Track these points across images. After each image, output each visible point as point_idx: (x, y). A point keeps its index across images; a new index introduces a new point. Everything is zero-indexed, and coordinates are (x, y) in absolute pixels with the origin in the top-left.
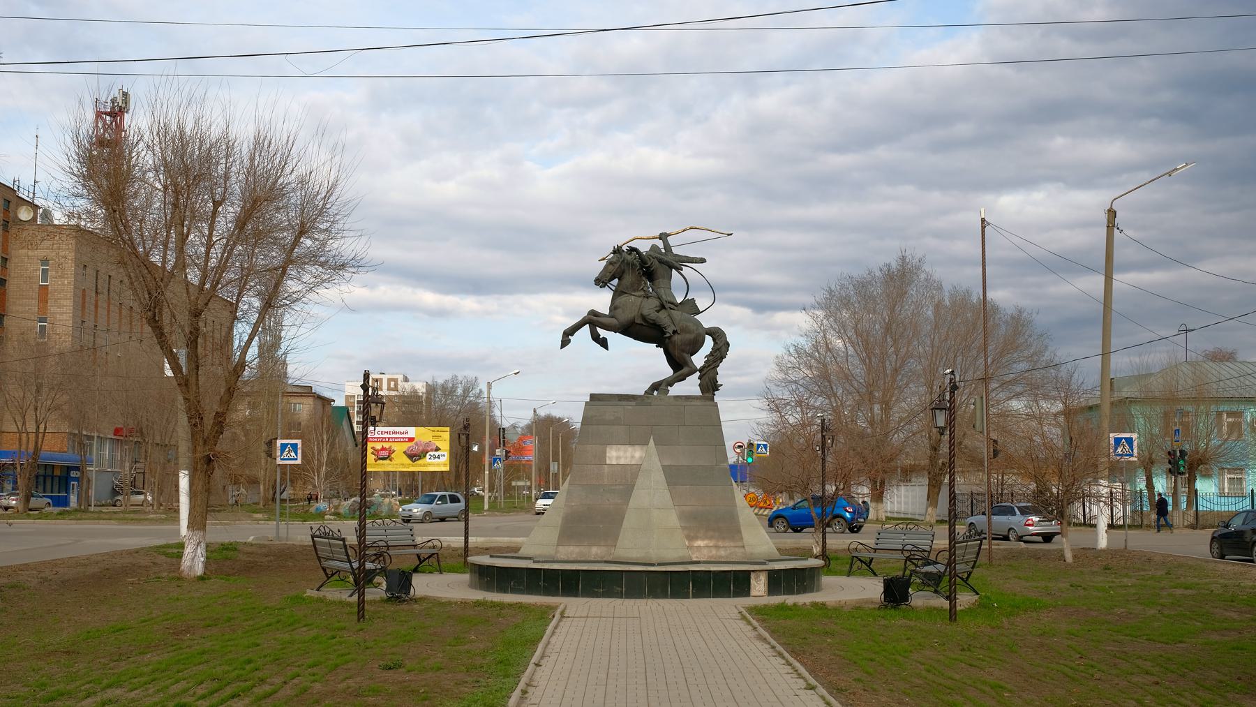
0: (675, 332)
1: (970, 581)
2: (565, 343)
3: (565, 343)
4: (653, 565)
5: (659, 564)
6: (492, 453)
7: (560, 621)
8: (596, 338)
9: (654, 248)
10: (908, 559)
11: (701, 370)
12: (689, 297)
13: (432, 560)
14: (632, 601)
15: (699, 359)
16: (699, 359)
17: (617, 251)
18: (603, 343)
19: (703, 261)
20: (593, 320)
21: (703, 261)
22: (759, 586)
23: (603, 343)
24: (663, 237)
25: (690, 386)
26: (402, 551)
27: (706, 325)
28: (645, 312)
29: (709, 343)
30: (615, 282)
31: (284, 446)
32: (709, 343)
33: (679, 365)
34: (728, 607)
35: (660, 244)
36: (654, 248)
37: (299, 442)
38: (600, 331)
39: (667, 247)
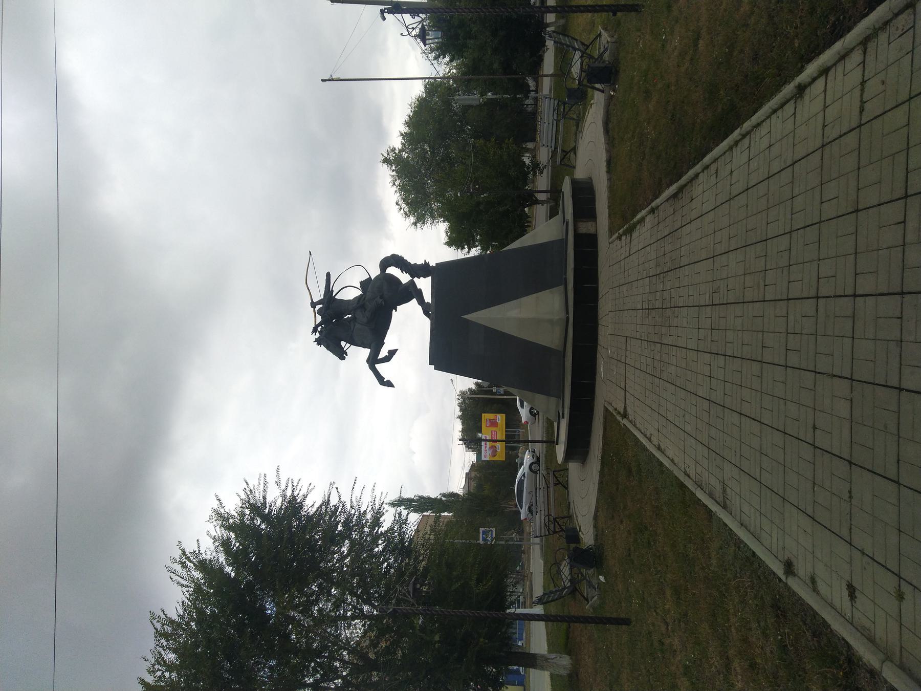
0: (381, 297)
1: (587, 43)
2: (389, 384)
3: (389, 384)
4: (568, 319)
5: (567, 312)
6: (495, 394)
7: (635, 425)
8: (387, 359)
9: (320, 312)
10: (564, 117)
11: (413, 276)
12: (358, 286)
13: (562, 528)
14: (600, 337)
15: (404, 278)
16: (404, 278)
17: (319, 342)
18: (392, 353)
19: (328, 275)
20: (373, 361)
21: (328, 275)
22: (586, 227)
23: (392, 353)
24: (313, 305)
25: (424, 284)
26: (552, 500)
27: (378, 272)
28: (365, 320)
29: (393, 271)
30: (343, 344)
31: (484, 539)
32: (393, 271)
33: (410, 293)
34: (611, 252)
35: (318, 307)
36: (320, 312)
37: (481, 530)
38: (381, 356)
39: (319, 303)
